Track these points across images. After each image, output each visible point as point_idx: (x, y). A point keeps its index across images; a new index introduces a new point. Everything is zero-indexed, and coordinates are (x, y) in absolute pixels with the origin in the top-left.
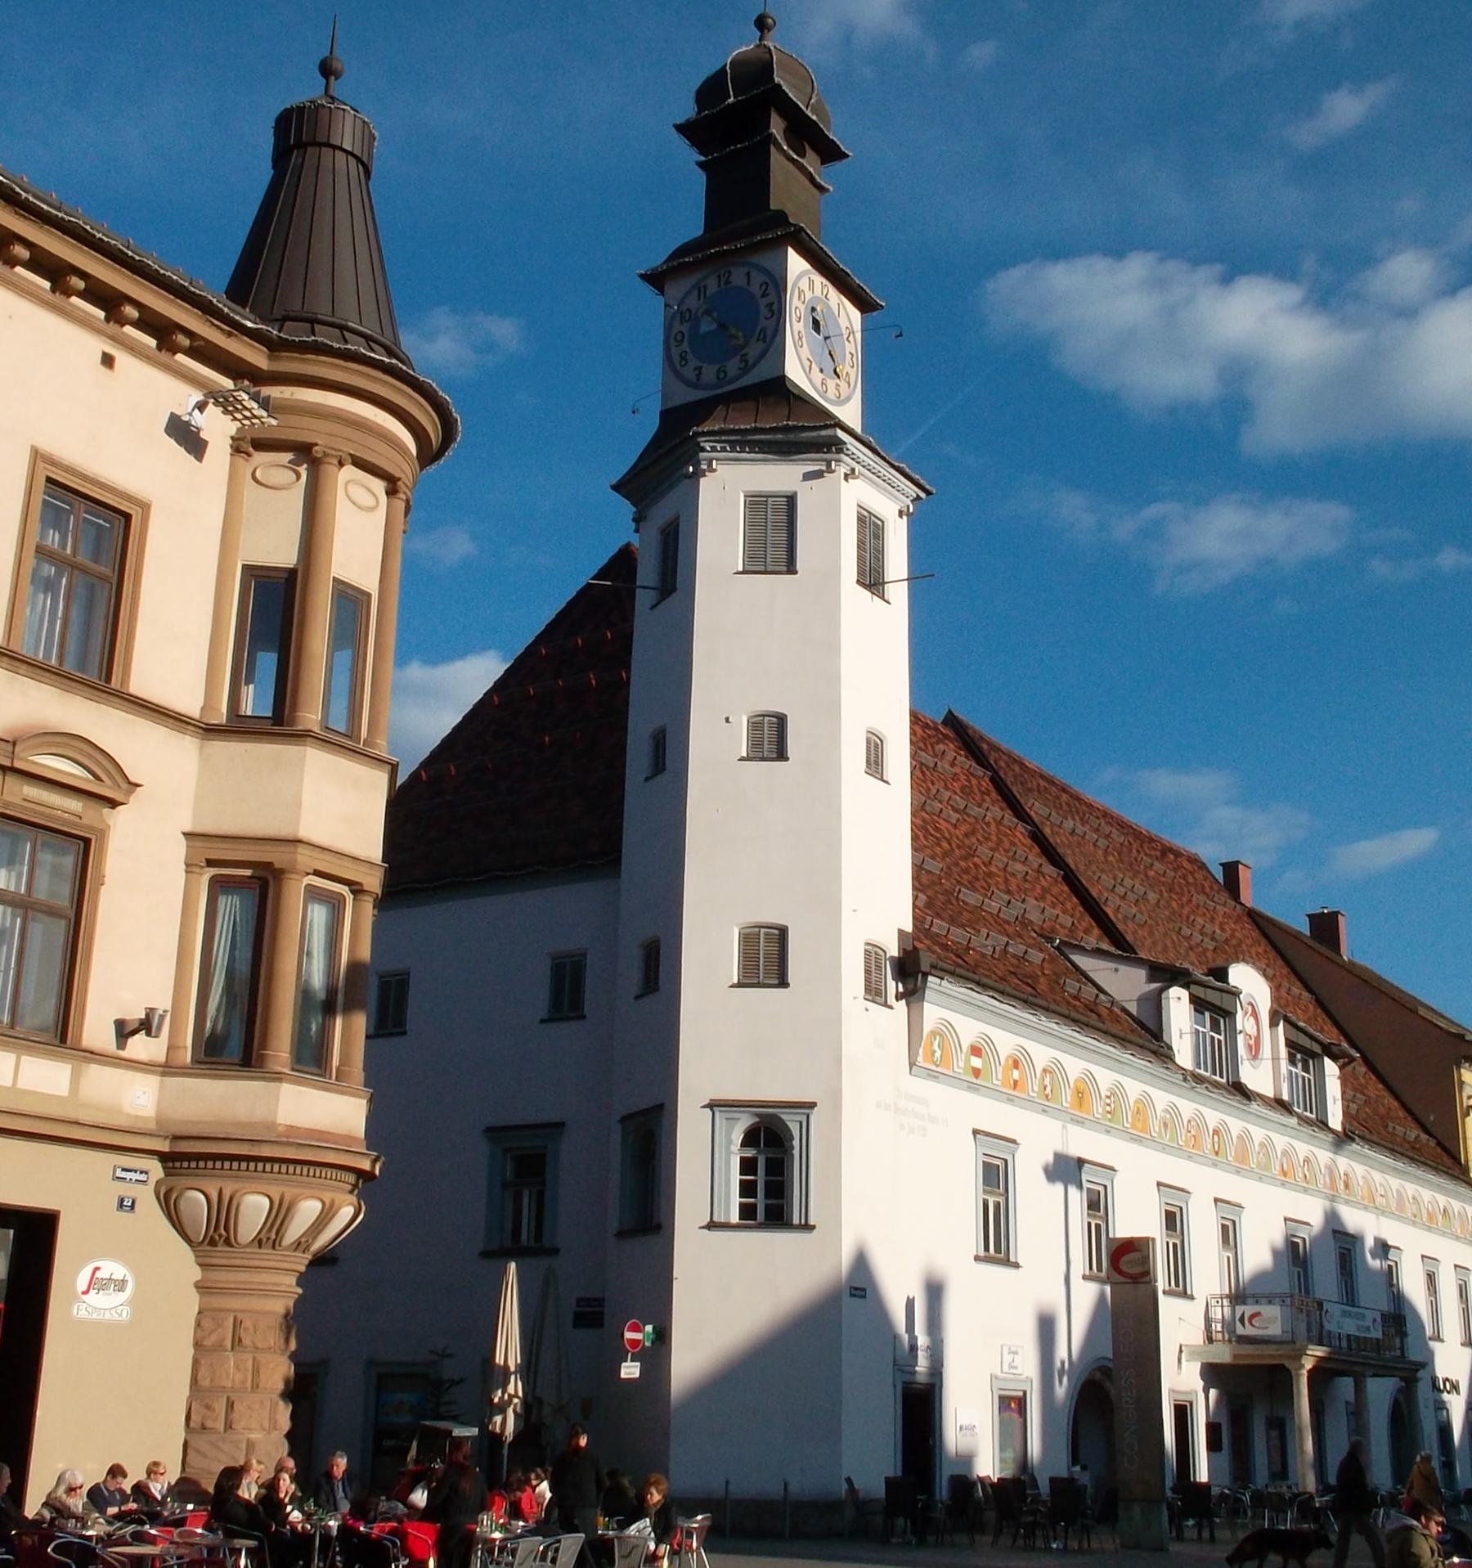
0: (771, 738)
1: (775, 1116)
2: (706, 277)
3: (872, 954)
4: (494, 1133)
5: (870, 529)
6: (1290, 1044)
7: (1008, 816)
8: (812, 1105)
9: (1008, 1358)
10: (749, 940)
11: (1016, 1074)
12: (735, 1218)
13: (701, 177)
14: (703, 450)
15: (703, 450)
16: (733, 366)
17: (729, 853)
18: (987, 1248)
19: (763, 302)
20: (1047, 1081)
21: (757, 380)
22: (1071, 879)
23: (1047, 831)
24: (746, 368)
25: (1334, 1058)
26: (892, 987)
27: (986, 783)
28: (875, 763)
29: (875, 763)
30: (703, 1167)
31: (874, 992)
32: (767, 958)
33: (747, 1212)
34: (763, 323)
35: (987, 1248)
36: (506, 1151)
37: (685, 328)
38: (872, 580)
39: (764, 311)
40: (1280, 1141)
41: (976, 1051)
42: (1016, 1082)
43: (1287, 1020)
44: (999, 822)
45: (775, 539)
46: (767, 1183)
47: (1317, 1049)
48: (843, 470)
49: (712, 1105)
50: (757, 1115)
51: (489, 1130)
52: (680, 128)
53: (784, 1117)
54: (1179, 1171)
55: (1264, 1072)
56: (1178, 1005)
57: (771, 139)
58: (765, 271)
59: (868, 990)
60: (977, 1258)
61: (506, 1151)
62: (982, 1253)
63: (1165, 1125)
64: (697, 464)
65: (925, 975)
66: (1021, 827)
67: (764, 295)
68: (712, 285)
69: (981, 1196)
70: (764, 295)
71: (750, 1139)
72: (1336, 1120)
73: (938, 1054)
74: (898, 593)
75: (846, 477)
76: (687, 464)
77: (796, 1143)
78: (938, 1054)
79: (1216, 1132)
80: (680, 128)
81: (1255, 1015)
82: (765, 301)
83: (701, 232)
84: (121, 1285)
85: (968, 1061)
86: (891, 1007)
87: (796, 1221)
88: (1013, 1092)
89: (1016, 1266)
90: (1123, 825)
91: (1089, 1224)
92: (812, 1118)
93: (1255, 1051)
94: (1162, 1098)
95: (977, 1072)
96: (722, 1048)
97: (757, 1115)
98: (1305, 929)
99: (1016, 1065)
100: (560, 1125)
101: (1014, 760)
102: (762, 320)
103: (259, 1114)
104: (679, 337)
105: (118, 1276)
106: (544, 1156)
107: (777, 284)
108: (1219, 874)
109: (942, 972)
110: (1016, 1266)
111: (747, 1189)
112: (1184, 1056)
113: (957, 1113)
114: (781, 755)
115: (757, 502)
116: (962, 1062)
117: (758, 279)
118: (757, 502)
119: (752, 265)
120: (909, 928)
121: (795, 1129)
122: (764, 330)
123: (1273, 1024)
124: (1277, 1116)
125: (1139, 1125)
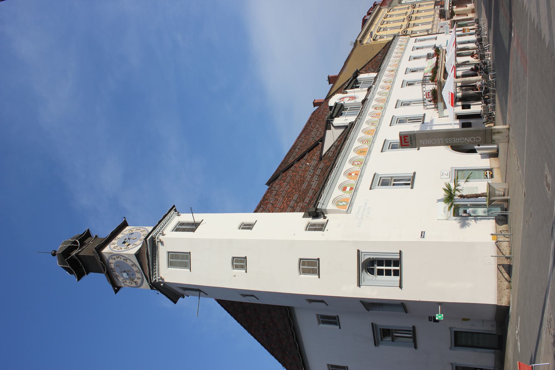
0: (240, 263)
1: (363, 264)
3: (311, 228)
4: (376, 344)
5: (182, 227)
6: (352, 88)
7: (292, 168)
8: (358, 251)
9: (445, 176)
10: (304, 271)
11: (353, 174)
12: (398, 278)
13: (91, 274)
14: (156, 281)
15: (156, 281)
16: (135, 269)
17: (275, 278)
18: (409, 184)
19: (117, 260)
20: (356, 163)
22: (309, 150)
23: (297, 157)
24: (134, 265)
25: (357, 76)
26: (321, 220)
27: (284, 174)
28: (248, 226)
29: (248, 226)
30: (379, 289)
31: (321, 228)
32: (310, 266)
33: (396, 273)
34: (122, 260)
35: (409, 184)
36: (382, 340)
38: (193, 227)
39: (119, 259)
40: (379, 90)
41: (344, 189)
42: (356, 174)
43: (346, 89)
44: (293, 171)
45: (181, 259)
46: (386, 266)
47: (354, 80)
48: (161, 237)
49: (359, 285)
50: (362, 271)
51: (375, 345)
53: (363, 261)
54: (387, 119)
55: (359, 94)
56: (337, 121)
57: (76, 255)
59: (321, 230)
60: (412, 188)
61: (382, 340)
62: (410, 186)
63: (373, 124)
64: (162, 283)
65: (317, 209)
66: (296, 165)
69: (392, 186)
71: (371, 272)
72: (374, 75)
73: (344, 203)
74: (198, 217)
75: (163, 235)
76: (160, 286)
77: (372, 257)
78: (344, 203)
79: (376, 109)
81: (343, 98)
85: (347, 192)
86: (328, 221)
87: (398, 257)
88: (359, 176)
89: (415, 173)
90: (301, 134)
92: (363, 251)
93: (353, 98)
94: (364, 126)
95: (351, 189)
96: (340, 282)
97: (362, 271)
98: (331, 85)
99: (350, 174)
100: (372, 324)
101: (280, 166)
106: (383, 329)
107: (112, 255)
108: (316, 108)
109: (317, 203)
111: (388, 273)
112: (352, 119)
113: (365, 195)
115: (171, 264)
116: (347, 195)
118: (171, 264)
120: (303, 214)
121: (367, 257)
123: (347, 93)
124: (372, 89)
125: (372, 132)
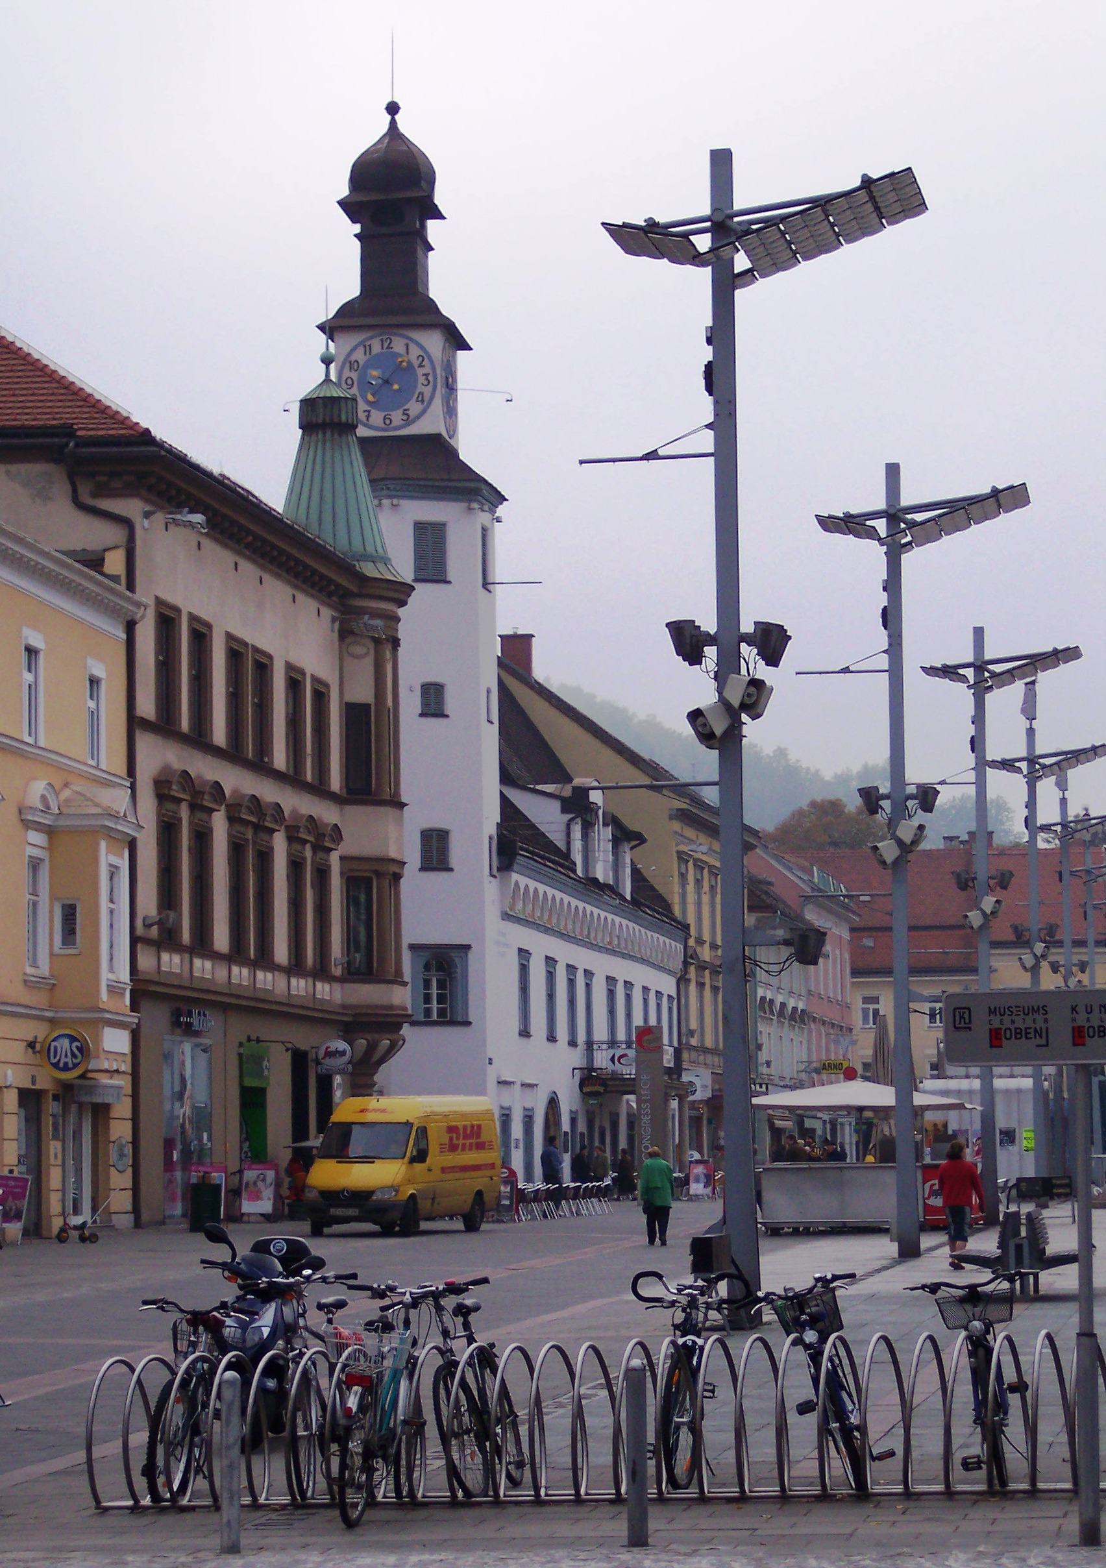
2: (371, 338)
19: (420, 371)
21: (417, 432)
24: (408, 421)
34: (420, 388)
37: (354, 375)
39: (422, 380)
52: (355, 236)
58: (422, 347)
67: (421, 366)
68: (376, 348)
70: (421, 366)
80: (355, 236)
82: (420, 371)
83: (357, 293)
84: (343, 1053)
91: (524, 954)
102: (420, 385)
103: (384, 1001)
104: (349, 382)
105: (341, 1049)
110: (447, 716)
114: (441, 714)
115: (421, 528)
117: (415, 352)
119: (411, 340)
122: (421, 394)
